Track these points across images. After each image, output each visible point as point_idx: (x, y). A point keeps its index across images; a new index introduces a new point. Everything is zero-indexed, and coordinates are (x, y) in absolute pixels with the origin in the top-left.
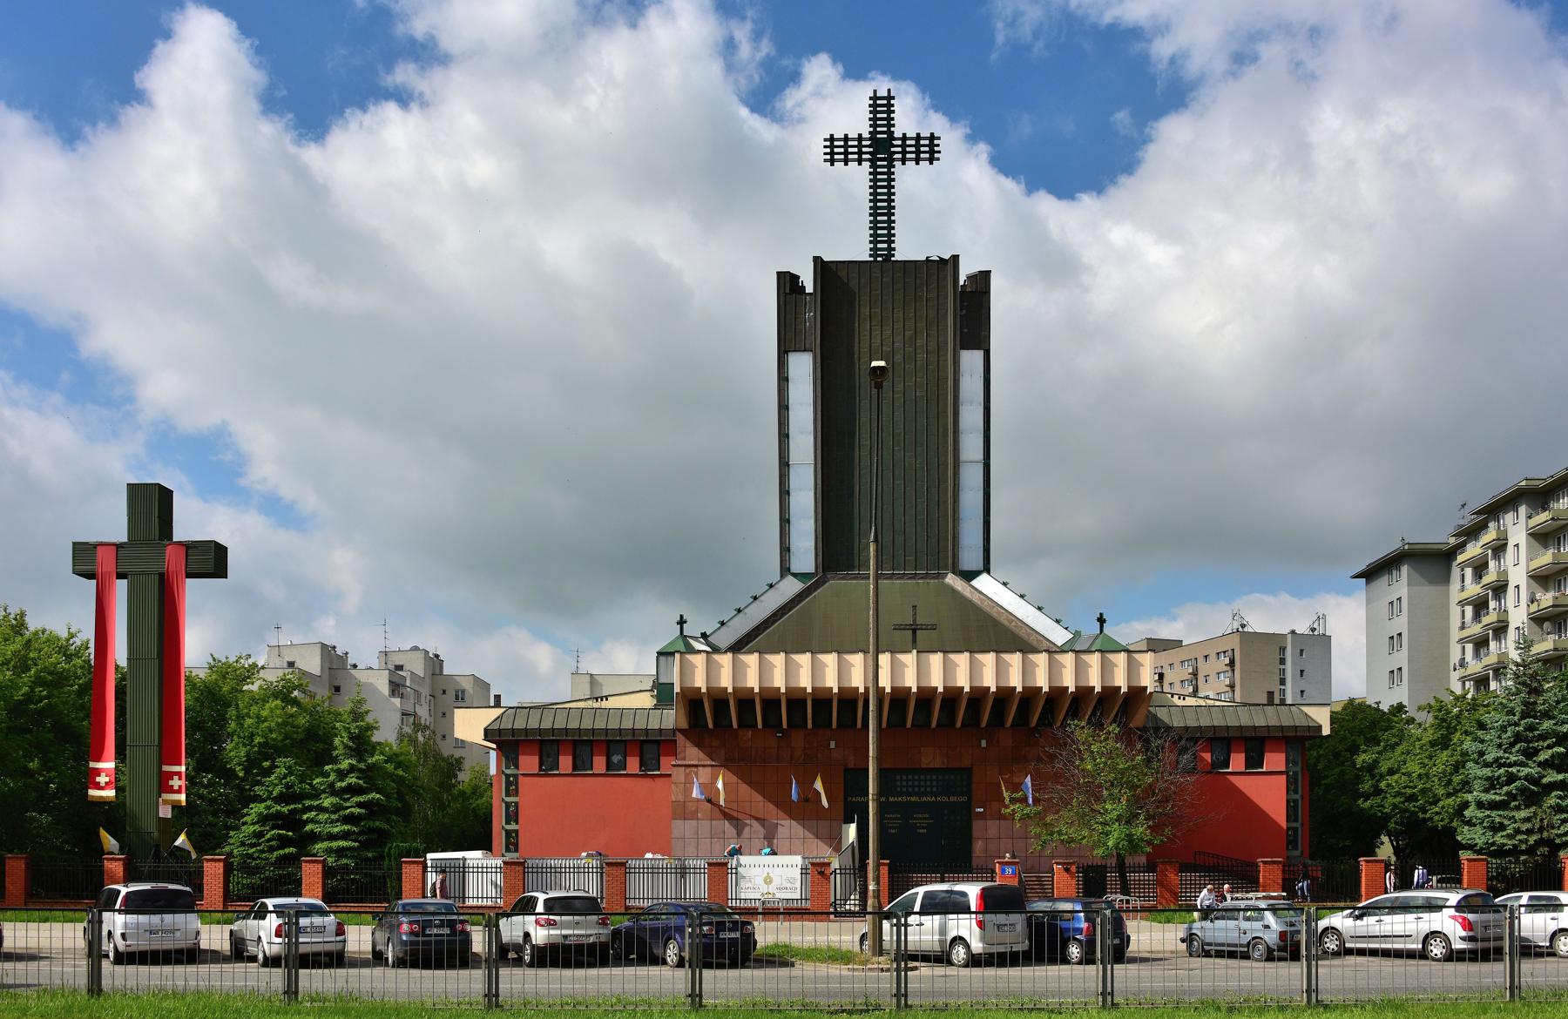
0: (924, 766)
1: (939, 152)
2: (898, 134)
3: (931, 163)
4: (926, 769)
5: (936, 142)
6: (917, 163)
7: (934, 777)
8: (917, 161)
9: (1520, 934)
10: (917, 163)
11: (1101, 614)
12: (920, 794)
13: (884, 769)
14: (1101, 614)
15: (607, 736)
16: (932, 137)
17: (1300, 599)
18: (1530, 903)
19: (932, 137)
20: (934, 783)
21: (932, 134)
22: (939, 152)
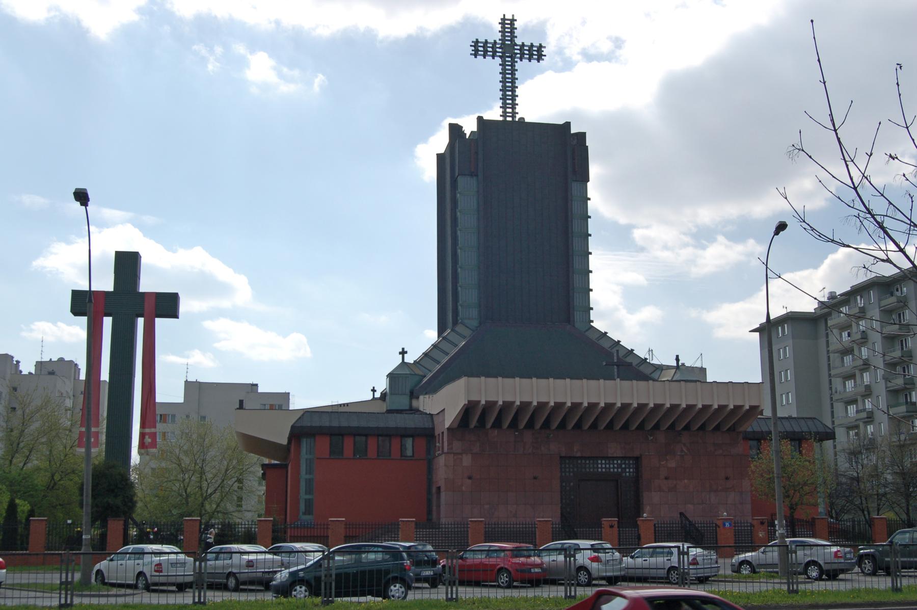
0: (610, 455)
1: (471, 46)
2: (498, 60)
3: (477, 40)
4: (611, 457)
5: (473, 52)
6: (486, 40)
7: (588, 470)
8: (486, 42)
9: (61, 574)
10: (485, 58)
11: (374, 388)
12: (745, 543)
13: (655, 538)
14: (374, 388)
15: (126, 581)
16: (476, 55)
17: (144, 236)
18: (271, 575)
19: (476, 55)
20: (600, 466)
21: (476, 57)
22: (471, 46)
